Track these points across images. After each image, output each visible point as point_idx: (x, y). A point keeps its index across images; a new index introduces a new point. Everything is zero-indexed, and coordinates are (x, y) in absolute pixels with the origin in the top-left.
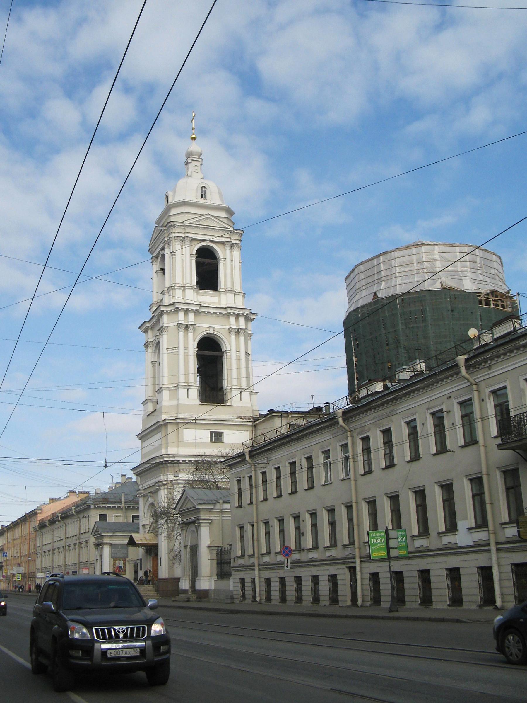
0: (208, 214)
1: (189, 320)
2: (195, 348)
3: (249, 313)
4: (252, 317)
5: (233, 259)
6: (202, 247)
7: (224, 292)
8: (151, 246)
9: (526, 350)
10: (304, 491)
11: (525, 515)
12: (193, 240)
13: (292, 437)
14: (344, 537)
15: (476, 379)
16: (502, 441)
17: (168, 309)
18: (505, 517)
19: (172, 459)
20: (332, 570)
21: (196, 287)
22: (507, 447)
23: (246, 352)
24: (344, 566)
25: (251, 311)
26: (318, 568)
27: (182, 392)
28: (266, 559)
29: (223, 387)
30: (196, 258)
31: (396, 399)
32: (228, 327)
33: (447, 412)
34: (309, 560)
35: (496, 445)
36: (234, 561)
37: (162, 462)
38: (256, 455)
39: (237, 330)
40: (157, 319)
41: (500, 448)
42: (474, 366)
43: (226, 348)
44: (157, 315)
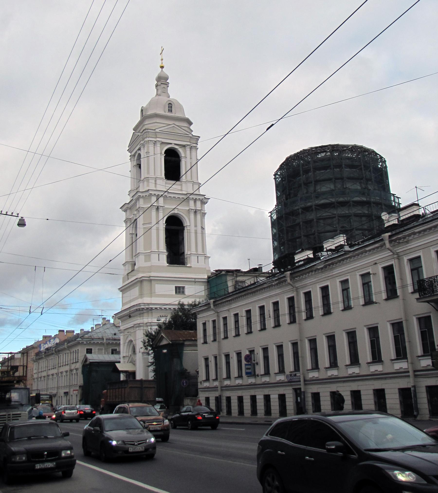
0: (174, 124)
1: (191, 206)
2: (164, 224)
3: (204, 198)
4: (205, 201)
5: (192, 158)
6: (171, 148)
7: (184, 182)
8: (130, 147)
9: (437, 229)
10: (259, 331)
11: (437, 350)
12: (163, 143)
13: (249, 292)
14: (289, 366)
15: (397, 250)
16: (420, 296)
17: (144, 194)
18: (419, 351)
19: (147, 307)
20: (282, 391)
21: (164, 178)
22: (423, 300)
23: (201, 227)
24: (291, 388)
25: (205, 196)
26: (284, 388)
27: (154, 257)
28: (227, 383)
29: (184, 253)
30: (165, 156)
31: (333, 264)
32: (188, 209)
33: (373, 274)
34: (262, 383)
35: (415, 299)
36: (201, 384)
37: (140, 309)
38: (218, 304)
39: (195, 210)
40: (135, 202)
41: (418, 301)
42: (395, 240)
43: (187, 224)
44: (135, 199)
